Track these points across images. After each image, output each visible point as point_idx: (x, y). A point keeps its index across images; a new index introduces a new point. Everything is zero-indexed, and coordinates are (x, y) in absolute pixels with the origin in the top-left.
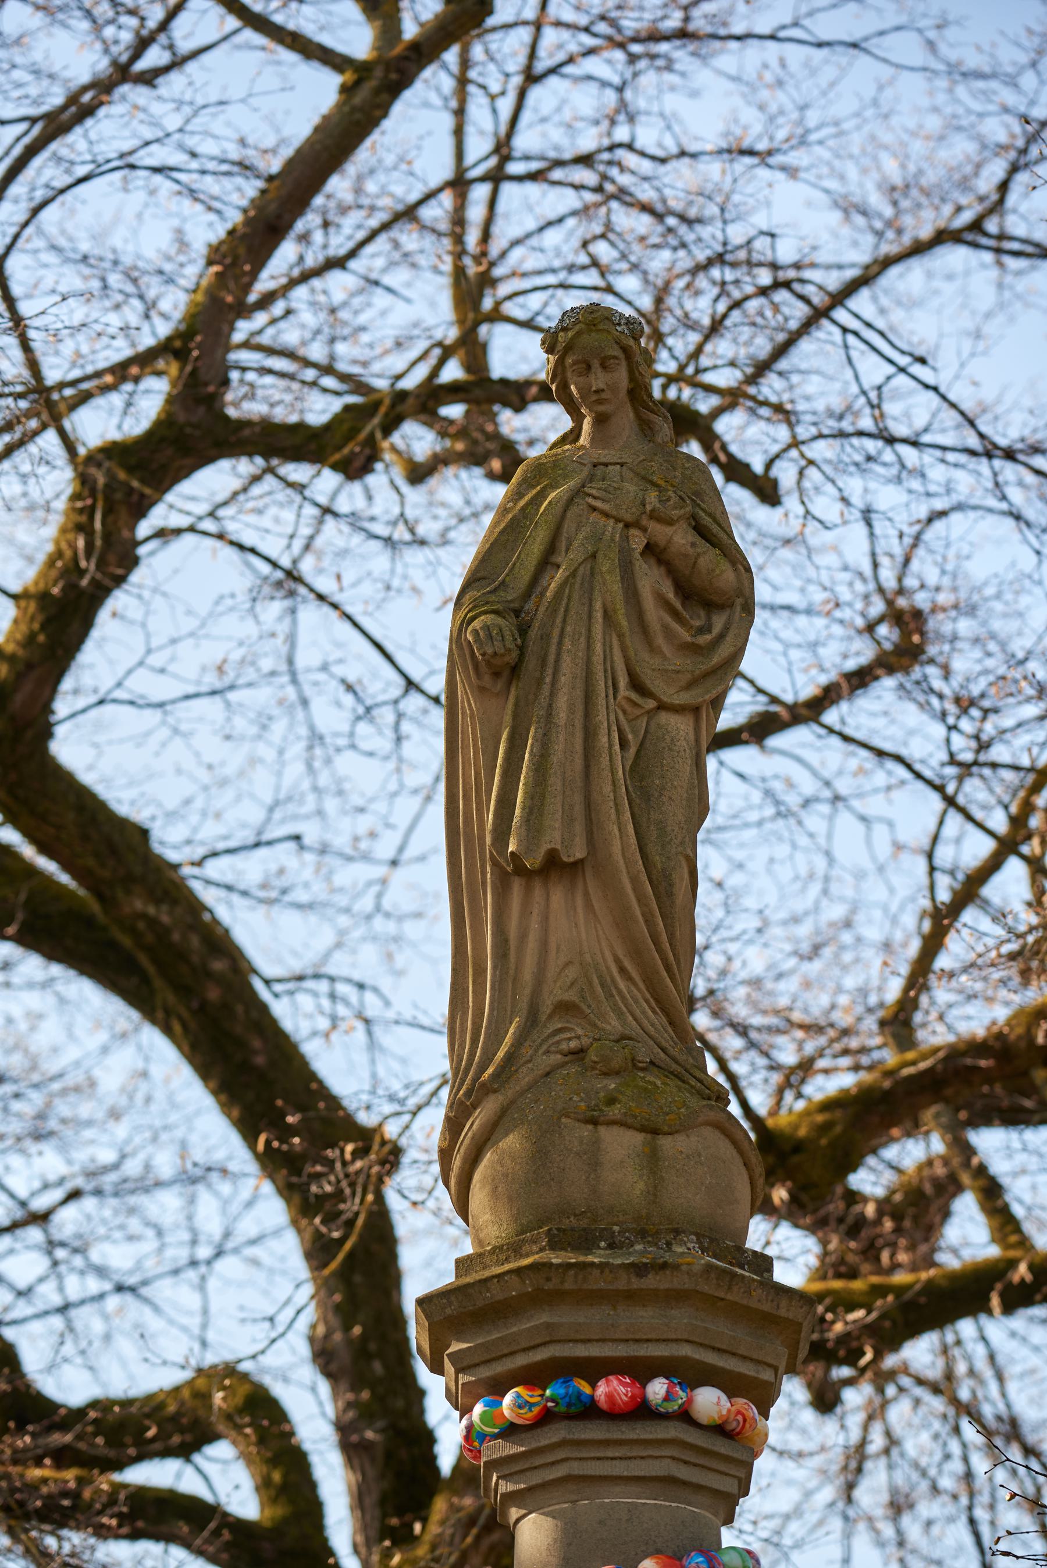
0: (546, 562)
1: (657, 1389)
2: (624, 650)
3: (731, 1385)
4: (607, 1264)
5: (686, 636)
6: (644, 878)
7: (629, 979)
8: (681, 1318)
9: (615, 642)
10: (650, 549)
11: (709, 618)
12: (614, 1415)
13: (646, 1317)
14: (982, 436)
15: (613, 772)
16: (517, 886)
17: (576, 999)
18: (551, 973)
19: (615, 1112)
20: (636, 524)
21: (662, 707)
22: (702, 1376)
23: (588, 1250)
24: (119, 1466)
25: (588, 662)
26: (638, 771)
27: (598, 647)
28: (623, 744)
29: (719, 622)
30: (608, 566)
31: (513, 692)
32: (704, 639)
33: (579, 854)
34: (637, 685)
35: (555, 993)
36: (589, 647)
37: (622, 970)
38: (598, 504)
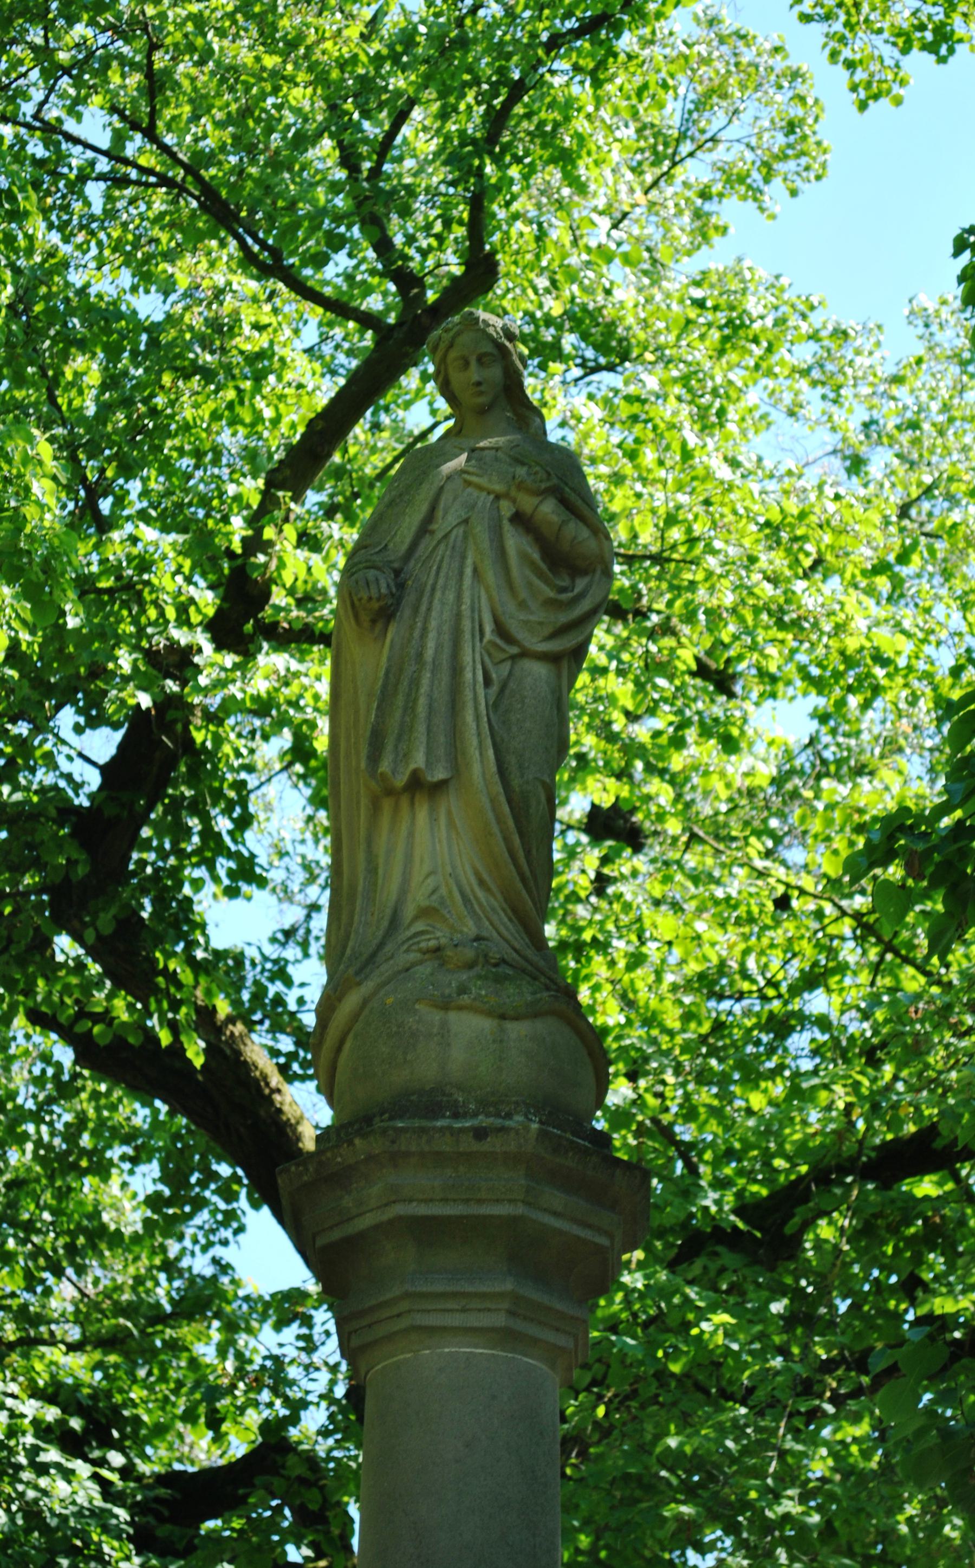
2: (490, 598)
4: (450, 1128)
5: (552, 594)
6: (503, 799)
7: (488, 890)
9: (483, 593)
10: (519, 519)
11: (573, 581)
14: (682, 160)
15: (476, 709)
16: (387, 805)
17: (436, 905)
18: (416, 878)
19: (465, 999)
20: (506, 496)
21: (525, 654)
23: (435, 1118)
25: (458, 616)
27: (467, 600)
28: (488, 682)
29: (581, 584)
30: (481, 531)
31: (389, 636)
32: (564, 597)
33: (440, 774)
34: (501, 630)
36: (459, 598)
37: (481, 882)
38: (474, 479)
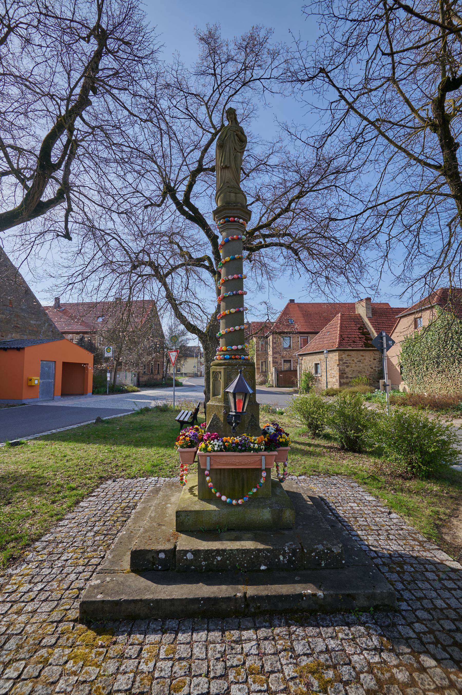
0: (225, 137)
1: (236, 219)
3: (244, 220)
8: (238, 211)
12: (231, 222)
13: (235, 211)
22: (240, 218)
24: (162, 336)
26: (235, 158)
30: (232, 135)
35: (226, 181)
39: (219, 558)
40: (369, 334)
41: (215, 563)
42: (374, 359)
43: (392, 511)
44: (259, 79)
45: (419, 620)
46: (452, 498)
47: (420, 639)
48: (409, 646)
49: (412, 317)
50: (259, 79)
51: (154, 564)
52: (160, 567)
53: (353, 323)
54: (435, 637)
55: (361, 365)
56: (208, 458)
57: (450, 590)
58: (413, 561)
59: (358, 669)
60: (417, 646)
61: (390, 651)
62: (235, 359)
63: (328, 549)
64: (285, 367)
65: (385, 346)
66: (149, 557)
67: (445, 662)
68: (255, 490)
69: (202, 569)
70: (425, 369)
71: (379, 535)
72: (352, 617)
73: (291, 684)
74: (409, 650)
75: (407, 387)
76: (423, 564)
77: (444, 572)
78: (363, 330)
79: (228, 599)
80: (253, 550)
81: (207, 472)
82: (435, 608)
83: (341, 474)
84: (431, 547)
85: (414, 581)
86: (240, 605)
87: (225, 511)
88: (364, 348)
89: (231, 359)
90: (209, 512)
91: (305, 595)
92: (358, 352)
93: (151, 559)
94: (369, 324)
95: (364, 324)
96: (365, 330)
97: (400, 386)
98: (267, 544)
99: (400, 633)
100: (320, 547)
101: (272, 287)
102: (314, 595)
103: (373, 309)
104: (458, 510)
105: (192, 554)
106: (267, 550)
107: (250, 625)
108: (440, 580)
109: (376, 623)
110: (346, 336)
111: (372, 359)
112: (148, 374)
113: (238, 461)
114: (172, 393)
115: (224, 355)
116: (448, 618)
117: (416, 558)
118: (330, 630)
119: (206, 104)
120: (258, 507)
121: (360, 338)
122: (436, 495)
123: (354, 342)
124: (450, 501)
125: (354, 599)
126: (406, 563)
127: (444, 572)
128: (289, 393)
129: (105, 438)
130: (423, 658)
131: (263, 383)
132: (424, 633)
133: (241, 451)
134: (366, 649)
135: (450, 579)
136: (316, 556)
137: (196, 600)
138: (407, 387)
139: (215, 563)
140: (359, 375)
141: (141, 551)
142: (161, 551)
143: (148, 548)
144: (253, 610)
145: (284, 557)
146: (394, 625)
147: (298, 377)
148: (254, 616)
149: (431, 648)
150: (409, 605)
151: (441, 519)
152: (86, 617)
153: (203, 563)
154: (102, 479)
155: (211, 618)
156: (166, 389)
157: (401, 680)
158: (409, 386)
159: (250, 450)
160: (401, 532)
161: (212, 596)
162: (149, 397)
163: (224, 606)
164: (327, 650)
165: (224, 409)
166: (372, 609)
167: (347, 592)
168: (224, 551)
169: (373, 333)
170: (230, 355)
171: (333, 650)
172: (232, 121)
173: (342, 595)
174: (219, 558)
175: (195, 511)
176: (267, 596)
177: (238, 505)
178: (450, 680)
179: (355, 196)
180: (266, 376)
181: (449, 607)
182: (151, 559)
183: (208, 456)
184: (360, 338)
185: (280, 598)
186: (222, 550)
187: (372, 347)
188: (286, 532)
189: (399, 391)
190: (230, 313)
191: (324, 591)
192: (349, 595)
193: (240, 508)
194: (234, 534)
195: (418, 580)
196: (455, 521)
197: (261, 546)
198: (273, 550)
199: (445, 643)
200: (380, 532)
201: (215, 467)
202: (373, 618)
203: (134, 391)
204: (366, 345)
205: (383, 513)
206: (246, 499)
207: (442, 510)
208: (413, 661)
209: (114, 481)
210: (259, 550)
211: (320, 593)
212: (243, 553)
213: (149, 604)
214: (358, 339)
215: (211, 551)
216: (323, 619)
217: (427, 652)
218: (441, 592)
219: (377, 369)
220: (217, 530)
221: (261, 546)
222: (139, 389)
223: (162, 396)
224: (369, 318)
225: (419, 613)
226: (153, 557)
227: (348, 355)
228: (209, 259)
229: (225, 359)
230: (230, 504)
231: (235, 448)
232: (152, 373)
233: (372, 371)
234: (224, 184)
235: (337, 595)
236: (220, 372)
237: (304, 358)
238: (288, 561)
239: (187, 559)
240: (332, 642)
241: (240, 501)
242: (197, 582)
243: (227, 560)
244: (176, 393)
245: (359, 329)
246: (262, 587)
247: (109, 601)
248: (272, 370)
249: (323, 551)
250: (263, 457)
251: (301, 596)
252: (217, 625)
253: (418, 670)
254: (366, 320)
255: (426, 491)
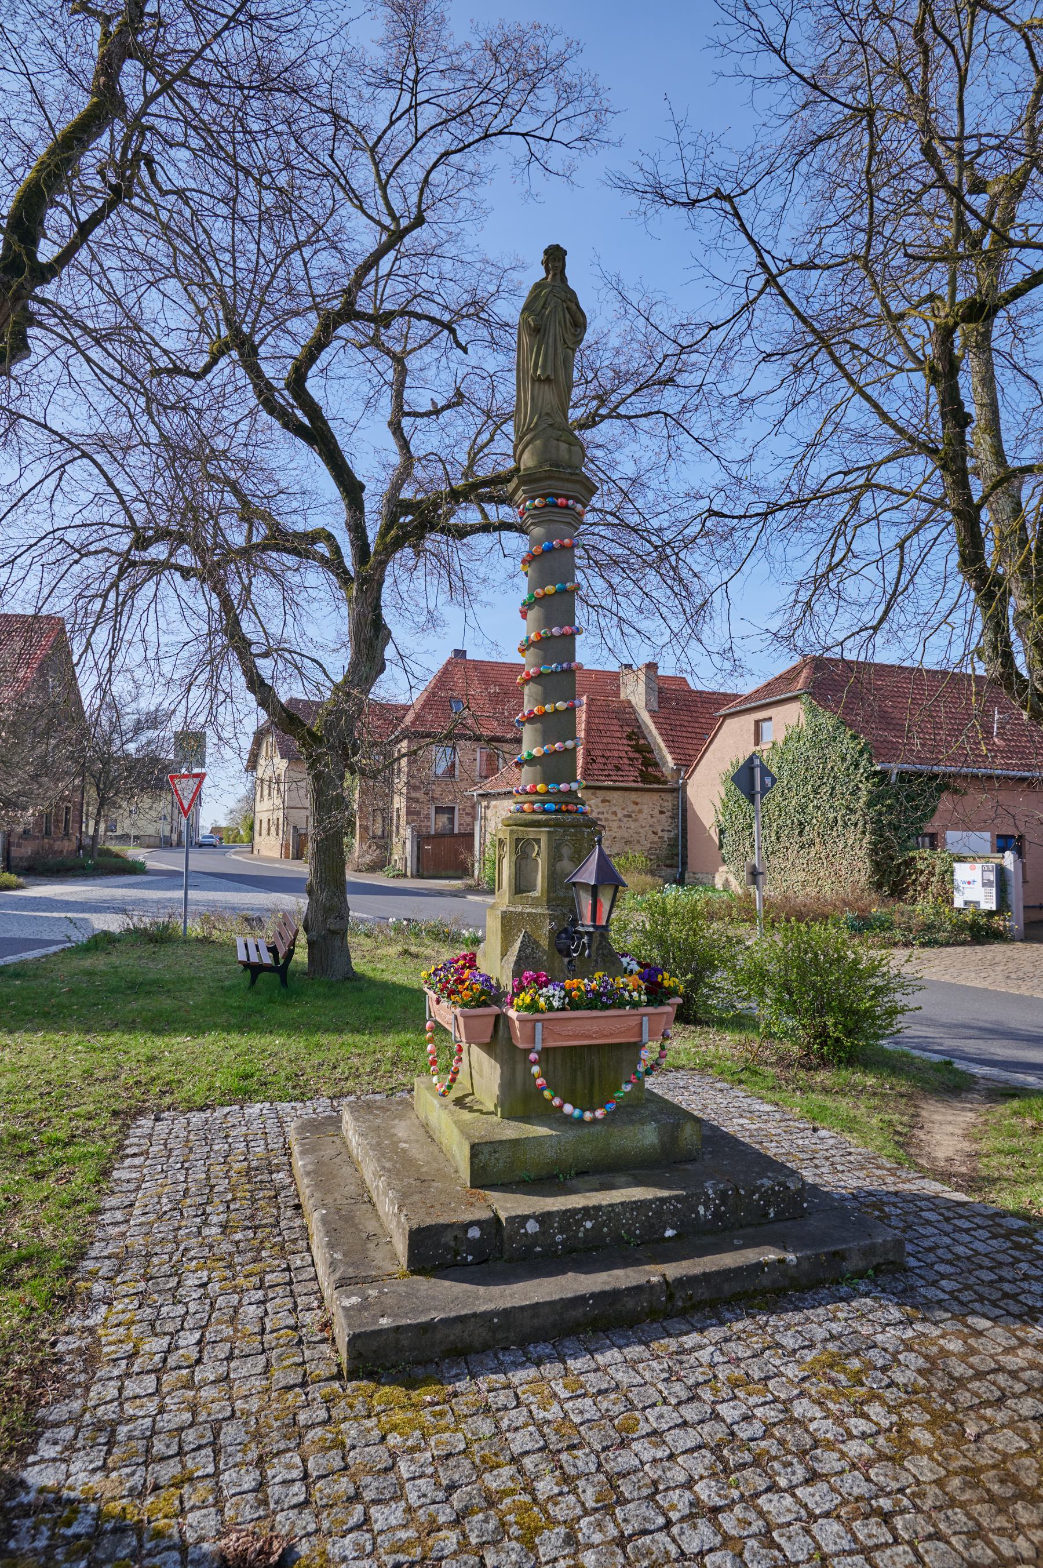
8: (578, 487)
13: (570, 485)
30: (560, 309)
39: (589, 1225)
40: (651, 752)
41: (581, 1235)
42: (661, 812)
43: (817, 1125)
44: (523, 135)
45: (943, 1276)
46: (902, 1096)
47: (957, 1299)
48: (946, 1310)
49: (750, 719)
50: (523, 135)
51: (457, 1253)
52: (470, 1258)
53: (615, 722)
54: (975, 1292)
55: (633, 825)
56: (539, 1025)
57: (967, 1231)
58: (893, 1199)
59: (891, 1350)
60: (957, 1308)
61: (924, 1320)
62: (568, 811)
63: (780, 1184)
64: (436, 823)
65: (758, 788)
66: (448, 1238)
67: (1003, 1319)
68: (628, 1088)
69: (556, 1251)
70: (773, 838)
71: (816, 1167)
72: (844, 1290)
73: (807, 1385)
74: (949, 1315)
75: (731, 878)
76: (911, 1201)
77: (948, 1209)
78: (637, 740)
79: (638, 1289)
80: (651, 1202)
81: (533, 1056)
82: (958, 1258)
83: (683, 1067)
84: (910, 1176)
85: (910, 1227)
86: (659, 1298)
87: (571, 1134)
88: (641, 785)
89: (557, 811)
90: (538, 1140)
91: (767, 1264)
92: (627, 794)
93: (452, 1243)
94: (652, 727)
95: (639, 727)
96: (642, 742)
97: (717, 876)
98: (671, 1189)
99: (925, 1297)
100: (767, 1183)
101: (474, 624)
102: (782, 1261)
103: (661, 691)
104: (918, 1116)
105: (537, 1221)
106: (677, 1198)
107: (684, 1327)
108: (947, 1220)
109: (883, 1291)
110: (599, 753)
111: (656, 812)
112: (37, 838)
113: (595, 1028)
114: (180, 894)
115: (544, 803)
116: (981, 1267)
117: (896, 1193)
118: (821, 1311)
119: (373, 150)
120: (632, 1122)
121: (630, 759)
122: (875, 1094)
123: (618, 769)
124: (903, 1101)
125: (844, 1259)
126: (884, 1204)
127: (948, 1209)
128: (455, 894)
129: (46, 1015)
130: (970, 1320)
131: (378, 866)
132: (959, 1291)
133: (605, 1007)
134: (887, 1325)
135: (961, 1217)
136: (760, 1200)
137: (579, 1300)
138: (731, 878)
139: (581, 1235)
140: (627, 848)
141: (429, 1228)
142: (472, 1224)
143: (442, 1220)
144: (680, 1304)
145: (707, 1208)
146: (913, 1288)
147: (477, 852)
148: (683, 1314)
149: (977, 1306)
150: (919, 1260)
151: (900, 1134)
152: (365, 1367)
153: (559, 1238)
154: (127, 1117)
155: (608, 1329)
156: (99, 881)
157: (956, 1351)
158: (736, 877)
159: (622, 1005)
160: (851, 1158)
161: (607, 1288)
162: (67, 903)
163: (630, 1303)
164: (833, 1337)
165: (551, 920)
166: (871, 1272)
167: (833, 1249)
168: (598, 1208)
169: (660, 749)
170: (556, 803)
171: (841, 1335)
172: (554, 275)
173: (826, 1254)
174: (589, 1225)
175: (510, 1141)
176: (704, 1274)
177: (594, 1121)
178: (1018, 1338)
179: (706, 443)
180: (386, 849)
181: (977, 1253)
182: (452, 1243)
183: (538, 1021)
184: (630, 759)
185: (726, 1274)
186: (594, 1207)
187: (659, 783)
188: (689, 1167)
189: (714, 889)
190: (556, 710)
191: (794, 1251)
192: (835, 1253)
193: (599, 1128)
194: (595, 1180)
195: (915, 1224)
196: (921, 1134)
197: (665, 1193)
198: (687, 1196)
199: (993, 1298)
200: (816, 1161)
201: (551, 1044)
202: (877, 1286)
203: (8, 888)
204: (645, 777)
205: (803, 1130)
206: (611, 1107)
207: (896, 1117)
208: (960, 1327)
209: (157, 1119)
210: (663, 1200)
211: (791, 1257)
212: (632, 1209)
213: (491, 1320)
214: (626, 761)
215: (574, 1212)
216: (802, 1300)
217: (974, 1313)
218: (956, 1236)
219: (666, 835)
220: (557, 1176)
221: (665, 1193)
222: (21, 880)
223: (104, 902)
224: (653, 713)
225: (941, 1268)
226: (456, 1238)
227: (603, 801)
228: (329, 538)
229: (545, 812)
230: (581, 1121)
231: (595, 1001)
232: (48, 833)
233: (656, 839)
234: (540, 417)
235: (817, 1256)
236: (538, 841)
237: (493, 803)
238: (713, 1214)
239: (526, 1234)
240: (833, 1325)
241: (599, 1113)
242: (563, 1272)
243: (604, 1226)
244: (193, 894)
245: (629, 738)
246: (684, 1263)
247: (410, 1325)
248: (407, 832)
249: (773, 1189)
250: (645, 1019)
251: (759, 1266)
252: (628, 1337)
253: (971, 1335)
254: (646, 717)
255: (854, 1087)
